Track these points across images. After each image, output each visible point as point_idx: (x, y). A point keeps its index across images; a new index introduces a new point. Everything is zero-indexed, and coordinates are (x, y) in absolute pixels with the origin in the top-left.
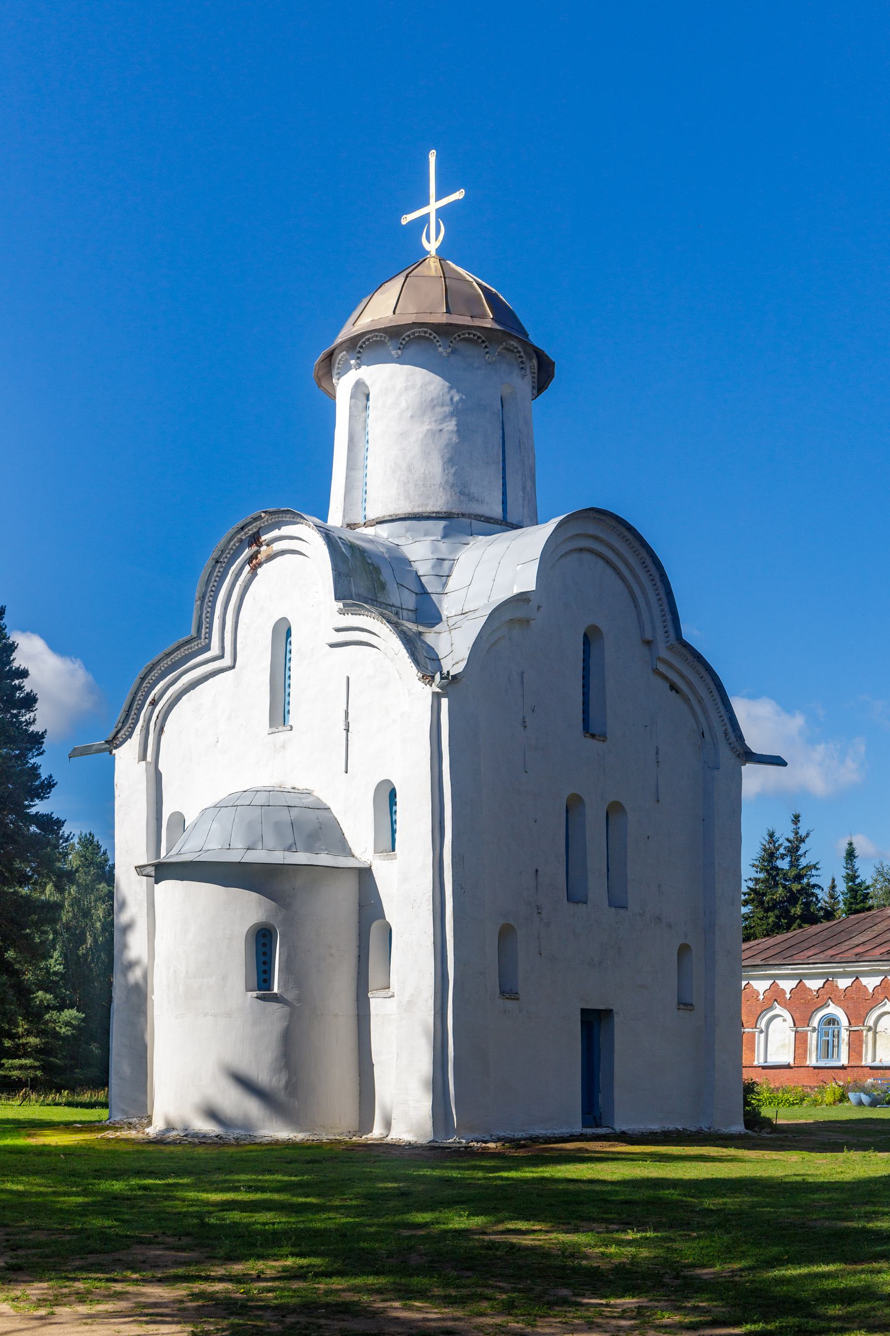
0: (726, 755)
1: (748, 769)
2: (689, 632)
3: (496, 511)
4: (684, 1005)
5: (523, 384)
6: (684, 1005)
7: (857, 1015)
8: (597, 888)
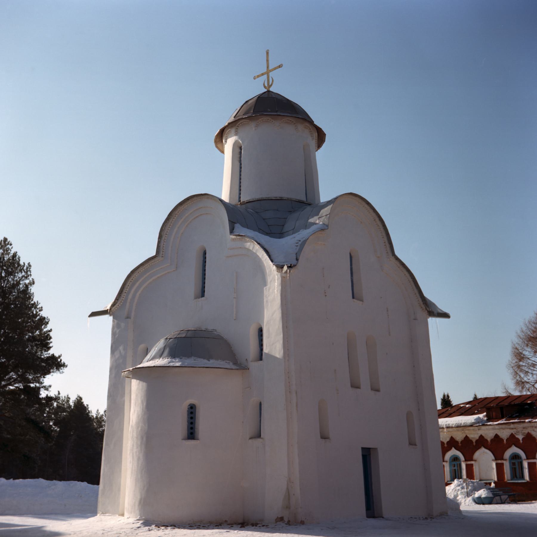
0: (421, 313)
1: (432, 322)
2: (397, 253)
3: (303, 198)
4: (412, 443)
5: (313, 143)
6: (412, 443)
7: (469, 457)
8: (365, 380)
